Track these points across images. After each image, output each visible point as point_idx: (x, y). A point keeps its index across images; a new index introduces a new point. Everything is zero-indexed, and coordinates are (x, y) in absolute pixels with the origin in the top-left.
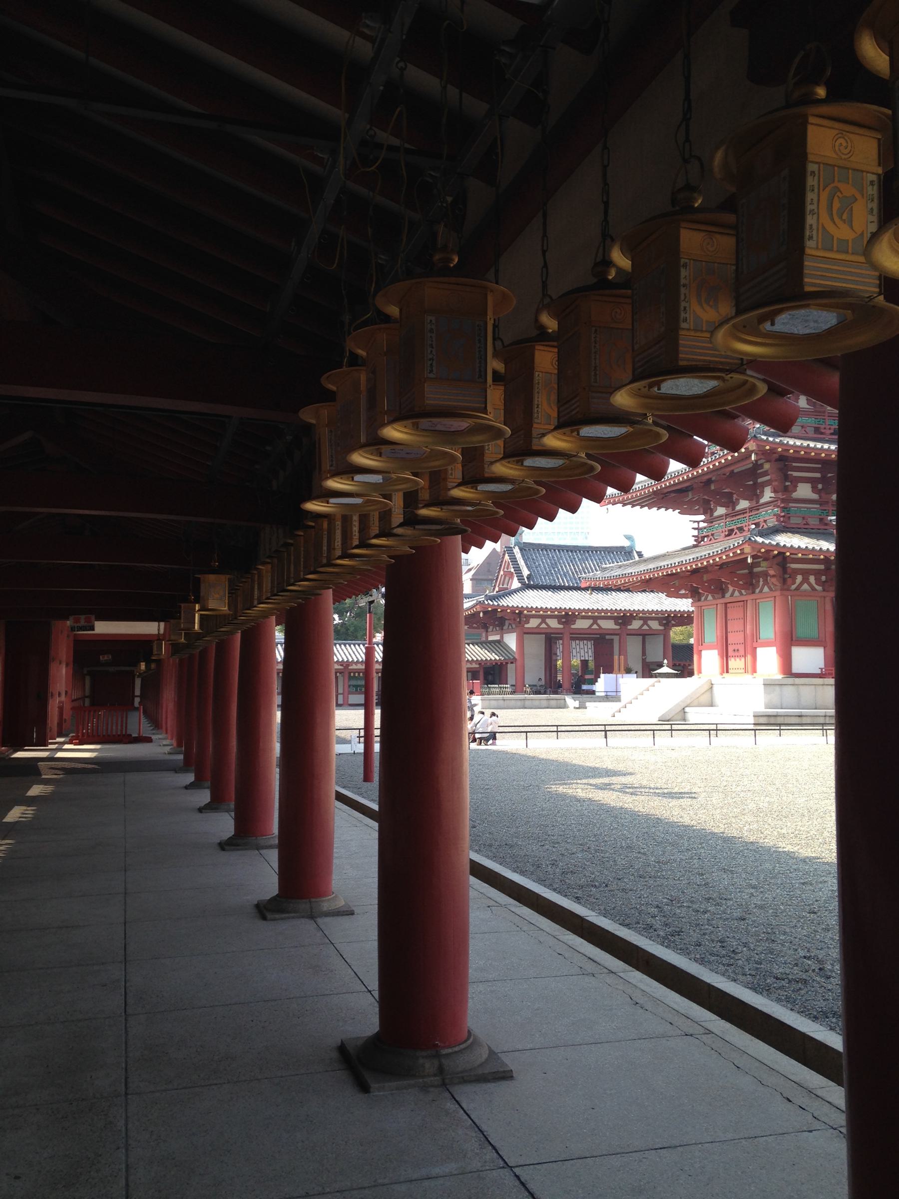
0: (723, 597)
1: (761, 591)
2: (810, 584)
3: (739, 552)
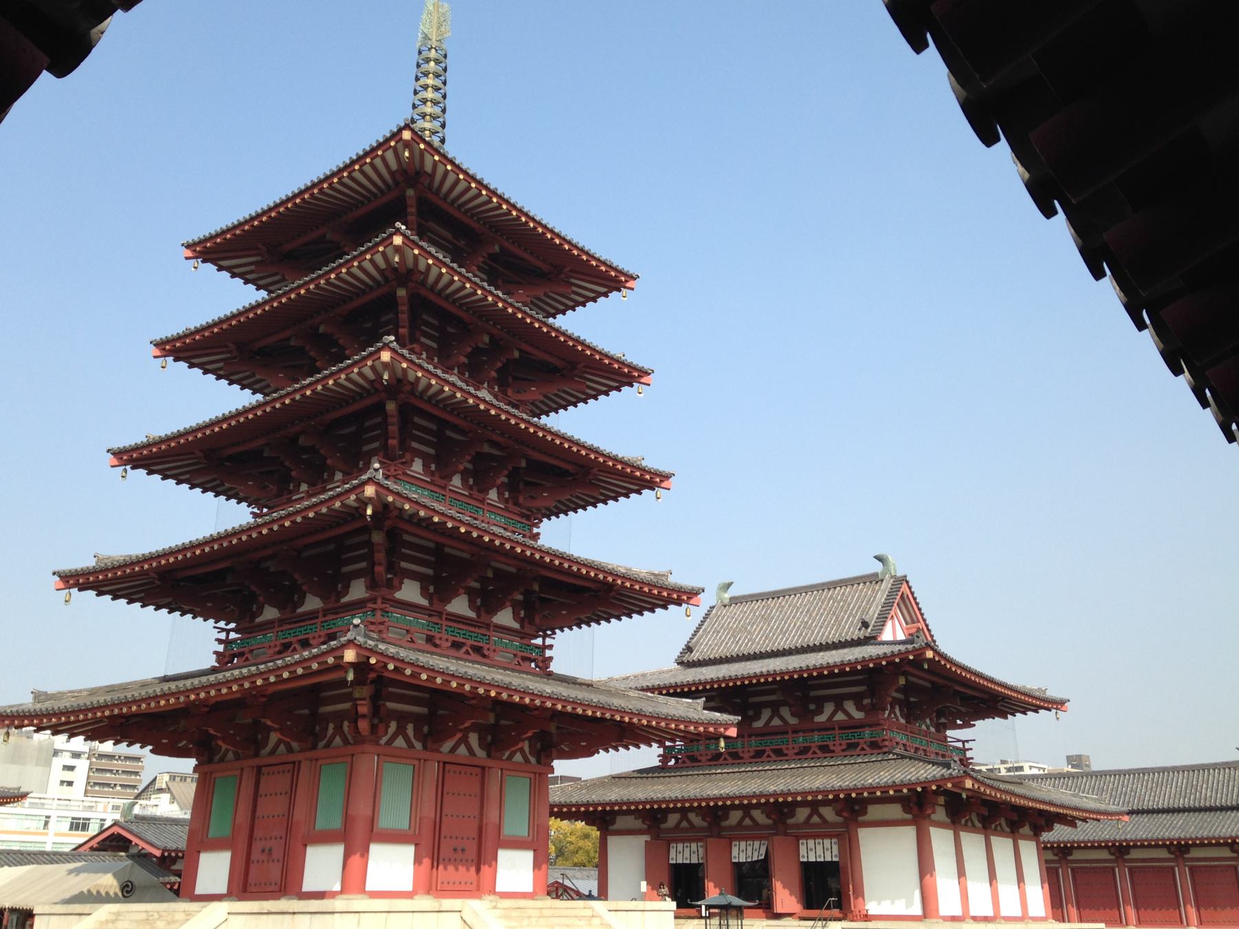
0: (257, 755)
1: (390, 742)
2: (782, 719)
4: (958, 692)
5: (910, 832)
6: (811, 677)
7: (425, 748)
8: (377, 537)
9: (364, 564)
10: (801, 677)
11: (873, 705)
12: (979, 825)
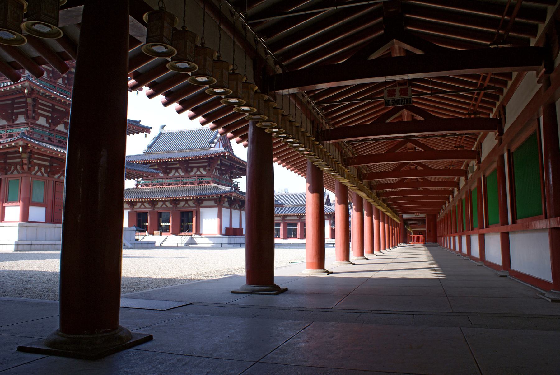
2: (179, 173)
3: (13, 144)
4: (237, 167)
5: (216, 210)
6: (189, 160)
7: (48, 176)
8: (29, 100)
9: (23, 110)
10: (185, 159)
11: (209, 170)
12: (238, 208)
